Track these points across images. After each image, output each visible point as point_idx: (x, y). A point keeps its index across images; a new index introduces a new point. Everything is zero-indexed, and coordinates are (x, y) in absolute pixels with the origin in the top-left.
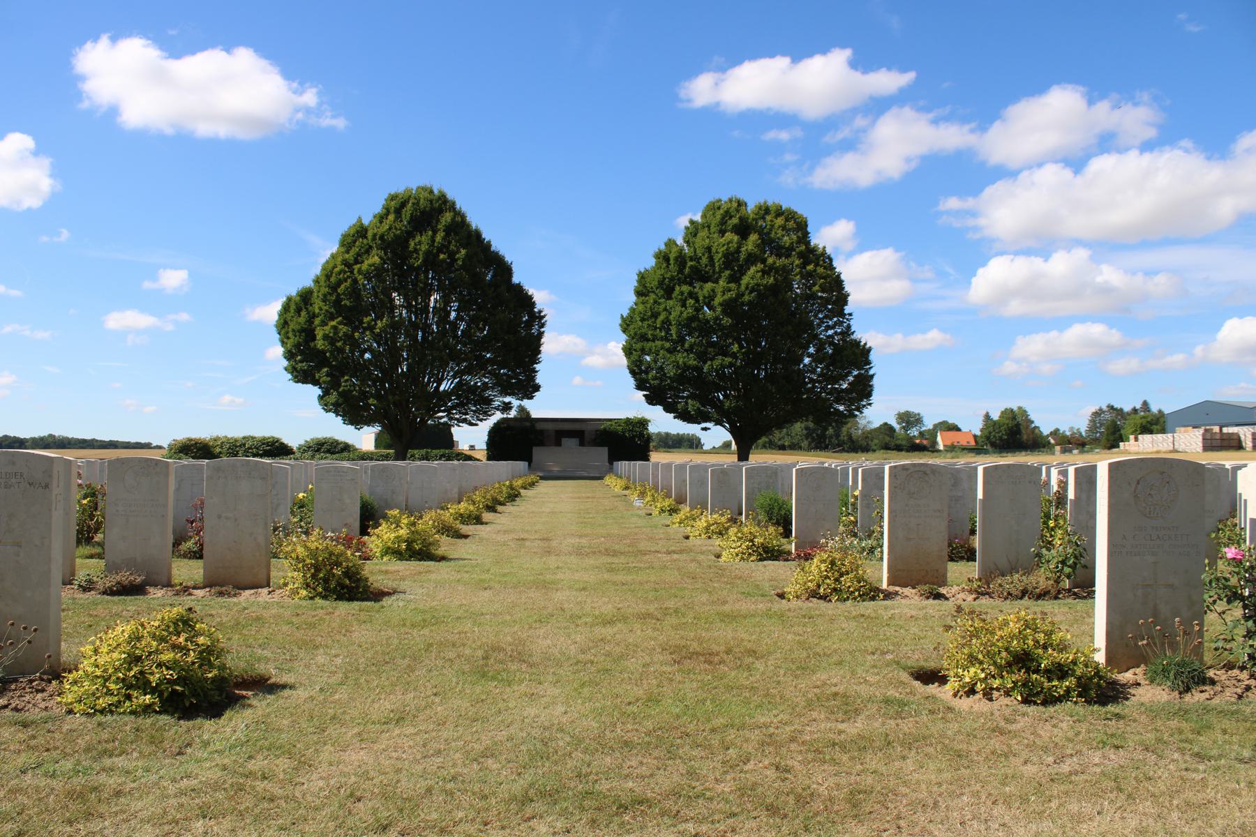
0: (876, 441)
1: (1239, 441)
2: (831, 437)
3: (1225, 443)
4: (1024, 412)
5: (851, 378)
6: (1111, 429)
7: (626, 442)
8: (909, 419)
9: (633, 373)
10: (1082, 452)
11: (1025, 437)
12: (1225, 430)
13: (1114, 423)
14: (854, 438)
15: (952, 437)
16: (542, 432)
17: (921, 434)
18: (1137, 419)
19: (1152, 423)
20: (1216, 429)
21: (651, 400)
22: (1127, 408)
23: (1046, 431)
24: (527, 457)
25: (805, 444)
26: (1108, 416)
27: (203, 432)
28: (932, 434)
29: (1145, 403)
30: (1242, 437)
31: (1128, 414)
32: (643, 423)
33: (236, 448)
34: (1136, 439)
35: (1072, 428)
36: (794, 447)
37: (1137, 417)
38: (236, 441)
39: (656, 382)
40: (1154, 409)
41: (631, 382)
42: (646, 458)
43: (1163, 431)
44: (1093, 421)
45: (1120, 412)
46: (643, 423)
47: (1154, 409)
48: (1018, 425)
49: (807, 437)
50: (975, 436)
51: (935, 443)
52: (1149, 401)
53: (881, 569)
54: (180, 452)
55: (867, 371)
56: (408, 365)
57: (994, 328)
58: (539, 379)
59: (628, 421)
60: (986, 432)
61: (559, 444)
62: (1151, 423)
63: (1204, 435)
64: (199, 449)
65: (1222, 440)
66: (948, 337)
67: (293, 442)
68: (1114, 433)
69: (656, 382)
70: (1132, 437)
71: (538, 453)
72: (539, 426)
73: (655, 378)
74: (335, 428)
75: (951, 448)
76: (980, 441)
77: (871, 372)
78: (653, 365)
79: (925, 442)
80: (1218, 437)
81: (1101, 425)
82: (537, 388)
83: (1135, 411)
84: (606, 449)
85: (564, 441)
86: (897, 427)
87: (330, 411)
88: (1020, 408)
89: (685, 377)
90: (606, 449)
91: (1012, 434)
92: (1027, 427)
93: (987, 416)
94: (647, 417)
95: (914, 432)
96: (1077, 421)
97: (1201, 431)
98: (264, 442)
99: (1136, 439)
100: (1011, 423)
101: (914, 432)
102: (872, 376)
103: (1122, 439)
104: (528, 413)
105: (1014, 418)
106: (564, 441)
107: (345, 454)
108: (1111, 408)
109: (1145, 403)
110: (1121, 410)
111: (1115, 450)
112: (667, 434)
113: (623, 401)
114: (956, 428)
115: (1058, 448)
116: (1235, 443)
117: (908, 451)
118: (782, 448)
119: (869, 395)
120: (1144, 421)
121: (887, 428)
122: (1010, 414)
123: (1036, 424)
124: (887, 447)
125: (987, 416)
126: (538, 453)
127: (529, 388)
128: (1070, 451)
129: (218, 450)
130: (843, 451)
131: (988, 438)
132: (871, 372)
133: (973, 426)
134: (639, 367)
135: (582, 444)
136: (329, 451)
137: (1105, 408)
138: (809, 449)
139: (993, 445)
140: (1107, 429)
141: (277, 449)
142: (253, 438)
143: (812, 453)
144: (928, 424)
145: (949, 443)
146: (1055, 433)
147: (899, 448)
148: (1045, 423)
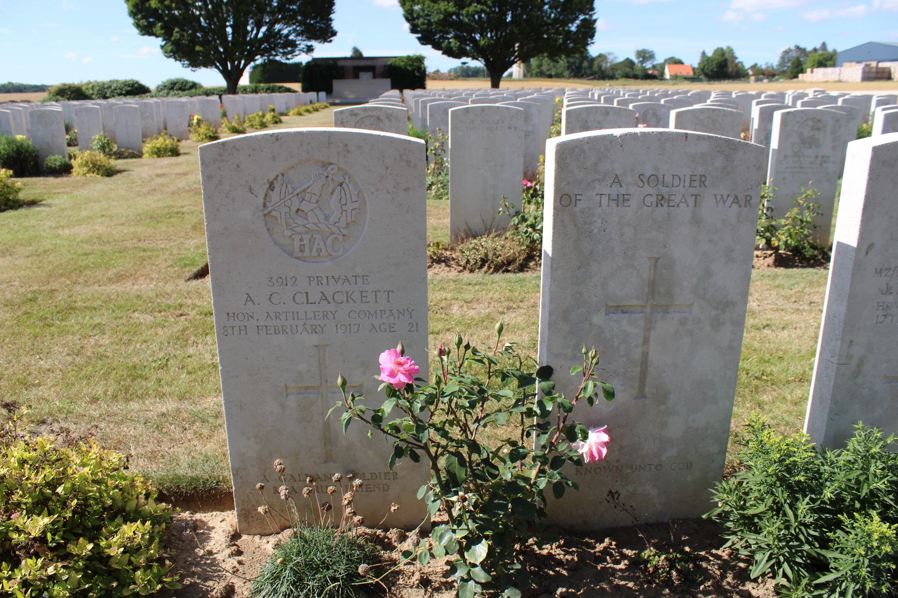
0: (619, 72)
1: (890, 73)
2: (586, 68)
3: (879, 75)
4: (731, 51)
5: (578, 22)
6: (795, 65)
7: (408, 75)
8: (645, 55)
9: (408, 20)
10: (770, 81)
11: (730, 69)
12: (881, 65)
13: (798, 58)
14: (603, 68)
15: (678, 69)
16: (343, 68)
17: (654, 67)
18: (816, 57)
19: (826, 60)
20: (874, 64)
21: (424, 40)
22: (809, 48)
23: (747, 65)
24: (329, 91)
25: (566, 73)
26: (794, 54)
27: (75, 78)
28: (662, 66)
29: (824, 45)
31: (810, 52)
32: (420, 59)
33: (104, 91)
34: (812, 72)
35: (767, 63)
36: (559, 76)
37: (816, 54)
38: (104, 84)
39: (425, 27)
40: (830, 49)
41: (407, 26)
42: (423, 87)
43: (834, 65)
44: (783, 58)
45: (802, 51)
46: (420, 59)
47: (830, 49)
48: (726, 61)
49: (568, 68)
50: (694, 69)
51: (662, 74)
54: (57, 94)
55: (591, 16)
56: (514, 47)
58: (335, 25)
59: (409, 58)
60: (702, 66)
61: (356, 77)
62: (826, 59)
63: (864, 69)
64: (72, 92)
65: (877, 72)
67: (152, 83)
68: (797, 67)
69: (425, 27)
70: (809, 70)
71: (337, 85)
72: (340, 63)
73: (423, 24)
74: (178, 70)
75: (675, 78)
76: (697, 71)
77: (594, 17)
78: (421, 14)
79: (656, 73)
80: (874, 70)
81: (789, 61)
82: (334, 34)
83: (815, 50)
85: (362, 74)
86: (636, 61)
87: (170, 57)
88: (728, 47)
89: (447, 22)
91: (721, 68)
92: (733, 62)
93: (704, 54)
94: (424, 54)
95: (648, 65)
96: (771, 58)
97: (862, 65)
98: (126, 84)
99: (812, 72)
100: (721, 59)
101: (648, 65)
102: (595, 21)
103: (802, 71)
104: (361, 54)
106: (362, 74)
107: (193, 91)
108: (798, 48)
109: (824, 45)
111: (795, 80)
113: (400, 43)
114: (680, 62)
115: (752, 78)
116: (886, 75)
118: (550, 76)
119: (592, 36)
120: (821, 58)
121: (629, 63)
122: (721, 52)
123: (740, 59)
124: (627, 76)
125: (704, 54)
126: (337, 85)
127: (326, 34)
128: (761, 80)
129: (91, 92)
130: (594, 79)
131: (703, 70)
132: (594, 17)
133: (692, 60)
134: (411, 14)
135: (374, 77)
136: (180, 89)
137: (793, 47)
138: (570, 77)
139: (706, 75)
140: (793, 64)
141: (137, 90)
142: (117, 81)
143: (572, 80)
144: (660, 59)
145: (673, 74)
146: (754, 67)
147: (636, 77)
148: (746, 58)
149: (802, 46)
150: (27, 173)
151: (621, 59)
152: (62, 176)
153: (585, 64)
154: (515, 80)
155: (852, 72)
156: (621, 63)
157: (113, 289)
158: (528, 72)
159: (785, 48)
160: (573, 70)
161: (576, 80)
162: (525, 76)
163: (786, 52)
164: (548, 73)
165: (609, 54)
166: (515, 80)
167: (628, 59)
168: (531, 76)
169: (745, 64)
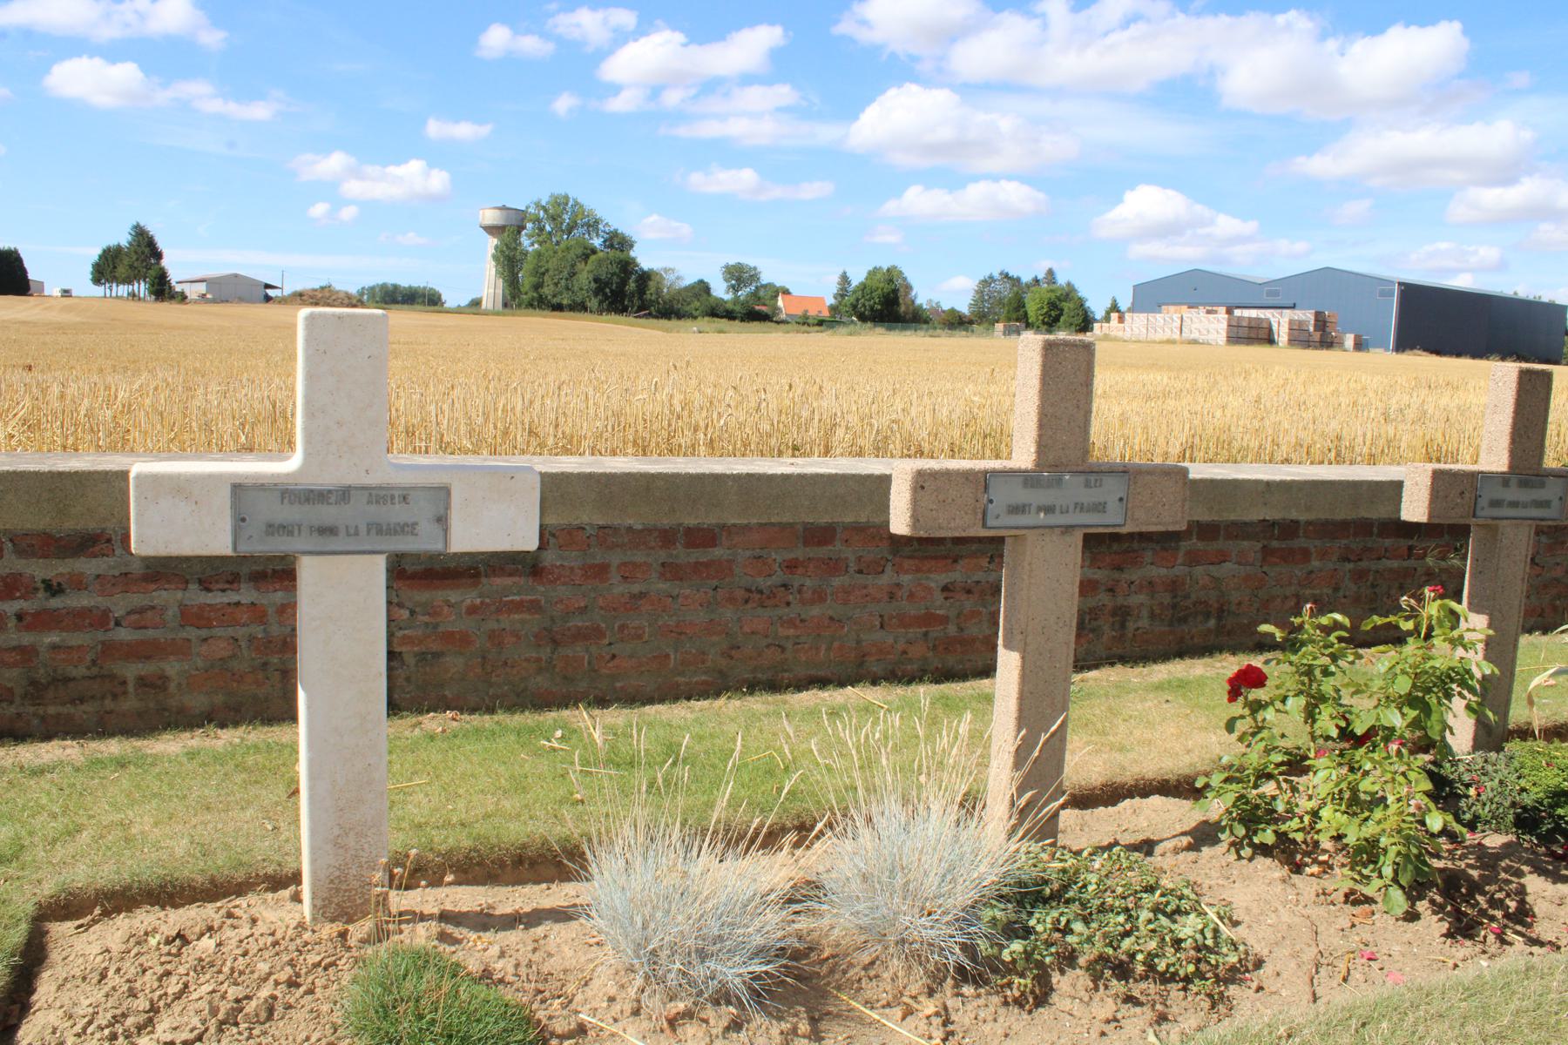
11: (902, 309)
22: (1026, 278)
25: (593, 303)
29: (1050, 272)
30: (1275, 328)
31: (1028, 286)
35: (930, 301)
40: (1062, 280)
44: (980, 292)
47: (1062, 280)
48: (895, 291)
52: (1055, 269)
53: (291, 374)
57: (872, 176)
66: (1041, 196)
83: (1036, 281)
84: (1505, 469)
88: (1069, 284)
90: (1505, 469)
100: (888, 288)
105: (891, 281)
108: (1007, 276)
109: (1050, 272)
110: (1018, 280)
112: (396, 287)
116: (1263, 334)
117: (742, 320)
118: (558, 308)
120: (1053, 296)
125: (845, 279)
130: (650, 315)
137: (996, 275)
138: (600, 312)
143: (605, 317)
149: (1013, 273)
150: (974, 630)
151: (689, 280)
152: (426, 552)
153: (632, 285)
154: (486, 313)
155: (580, 266)
156: (688, 289)
157: (68, 709)
158: (514, 298)
159: (984, 274)
160: (606, 297)
161: (614, 317)
162: (505, 305)
163: (987, 282)
164: (555, 301)
165: (666, 270)
166: (486, 313)
167: (701, 282)
168: (519, 306)
169: (958, 308)
